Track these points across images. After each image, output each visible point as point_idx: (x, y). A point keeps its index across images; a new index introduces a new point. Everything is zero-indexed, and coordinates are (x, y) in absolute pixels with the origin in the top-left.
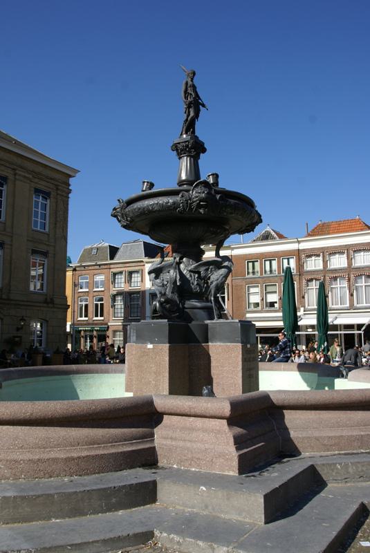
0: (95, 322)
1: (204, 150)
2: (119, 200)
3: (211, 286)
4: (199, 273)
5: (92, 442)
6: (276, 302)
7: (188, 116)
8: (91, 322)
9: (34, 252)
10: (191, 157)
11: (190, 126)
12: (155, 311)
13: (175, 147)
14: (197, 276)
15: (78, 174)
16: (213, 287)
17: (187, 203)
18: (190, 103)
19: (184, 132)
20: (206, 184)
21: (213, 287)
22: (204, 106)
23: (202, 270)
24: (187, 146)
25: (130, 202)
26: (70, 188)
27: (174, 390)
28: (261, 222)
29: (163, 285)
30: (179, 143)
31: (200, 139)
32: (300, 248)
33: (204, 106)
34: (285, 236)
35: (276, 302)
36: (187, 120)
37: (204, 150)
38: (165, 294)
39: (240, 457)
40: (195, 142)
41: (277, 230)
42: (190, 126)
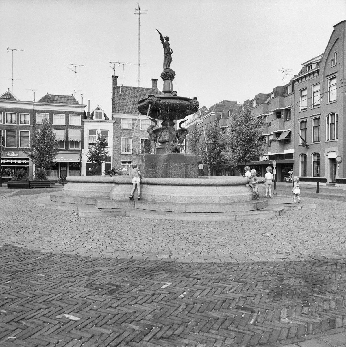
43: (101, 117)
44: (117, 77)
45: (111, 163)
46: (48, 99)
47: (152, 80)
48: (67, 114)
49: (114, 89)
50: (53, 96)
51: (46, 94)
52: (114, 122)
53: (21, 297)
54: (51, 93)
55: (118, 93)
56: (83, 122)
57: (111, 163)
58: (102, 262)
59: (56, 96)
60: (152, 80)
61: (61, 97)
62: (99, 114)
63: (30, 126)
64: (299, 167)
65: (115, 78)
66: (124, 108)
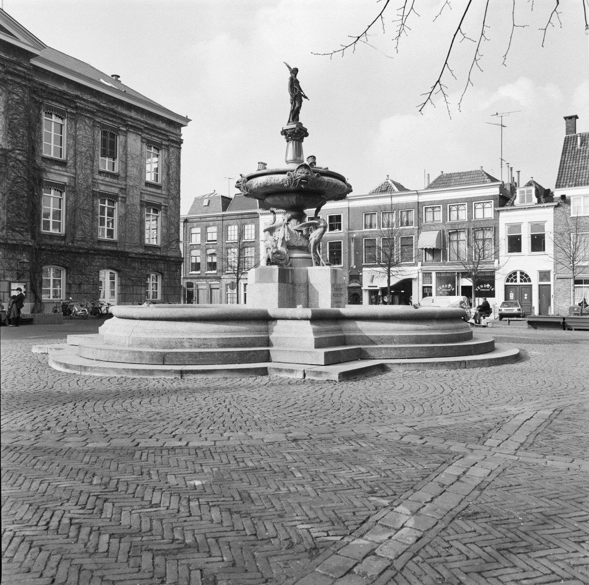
0: (208, 275)
1: (307, 135)
2: (241, 175)
3: (311, 241)
4: (302, 231)
5: (232, 332)
6: (60, 231)
7: (294, 107)
8: (203, 275)
9: (254, 242)
10: (296, 140)
11: (295, 114)
12: (269, 260)
13: (284, 132)
14: (300, 233)
15: (189, 123)
16: (312, 243)
17: (292, 180)
18: (296, 96)
19: (291, 120)
20: (306, 166)
21: (312, 243)
22: (306, 97)
23: (304, 229)
24: (294, 132)
25: (249, 178)
26: (182, 138)
27: (282, 305)
28: (352, 191)
29: (275, 241)
30: (287, 130)
31: (304, 126)
32: (420, 201)
33: (306, 97)
34: (406, 187)
35: (60, 231)
36: (293, 110)
37: (307, 135)
38: (276, 247)
39: (316, 339)
40: (300, 129)
41: (397, 181)
42: (295, 114)
43: (530, 200)
44: (576, 117)
45: (551, 283)
46: (444, 181)
47: (565, 118)
48: (470, 201)
49: (567, 140)
50: (450, 176)
51: (441, 174)
52: (556, 206)
53: (459, 543)
54: (447, 171)
55: (574, 148)
56: (497, 213)
57: (551, 283)
58: (91, 252)
59: (455, 175)
60: (565, 118)
61: (461, 175)
62: (526, 194)
63: (413, 229)
64: (236, 210)
65: (571, 120)
66: (578, 176)
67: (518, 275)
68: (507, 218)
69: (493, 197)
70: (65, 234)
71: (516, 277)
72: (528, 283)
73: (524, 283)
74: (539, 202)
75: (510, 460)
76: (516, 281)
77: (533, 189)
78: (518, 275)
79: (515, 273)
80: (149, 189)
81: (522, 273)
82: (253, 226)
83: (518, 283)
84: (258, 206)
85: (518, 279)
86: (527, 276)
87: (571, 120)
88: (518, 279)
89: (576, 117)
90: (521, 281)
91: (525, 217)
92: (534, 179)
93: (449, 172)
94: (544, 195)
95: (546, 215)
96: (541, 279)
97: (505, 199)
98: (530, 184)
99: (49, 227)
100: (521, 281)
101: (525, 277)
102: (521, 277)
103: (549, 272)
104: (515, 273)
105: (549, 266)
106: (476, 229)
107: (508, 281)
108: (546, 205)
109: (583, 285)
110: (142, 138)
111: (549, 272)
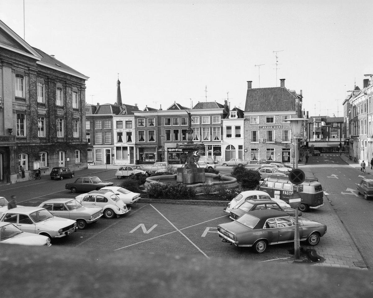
15: (89, 79)
47: (247, 82)
51: (198, 102)
65: (250, 83)
67: (231, 147)
68: (226, 123)
69: (221, 114)
70: (26, 136)
71: (229, 147)
72: (234, 150)
73: (232, 150)
74: (239, 117)
75: (277, 258)
76: (229, 149)
77: (236, 112)
78: (231, 147)
79: (229, 146)
80: (18, 102)
81: (232, 146)
82: (110, 122)
83: (230, 150)
84: (112, 112)
85: (231, 148)
86: (234, 147)
87: (250, 83)
88: (231, 148)
89: (285, 79)
90: (232, 149)
91: (233, 122)
92: (236, 107)
93: (202, 102)
94: (241, 114)
95: (240, 123)
96: (239, 149)
97: (225, 115)
98: (234, 109)
99: (20, 126)
100: (232, 149)
101: (233, 148)
102: (232, 148)
103: (242, 146)
104: (229, 146)
105: (242, 143)
106: (213, 127)
107: (226, 149)
108: (241, 119)
109: (255, 151)
110: (12, 69)
111: (242, 146)
